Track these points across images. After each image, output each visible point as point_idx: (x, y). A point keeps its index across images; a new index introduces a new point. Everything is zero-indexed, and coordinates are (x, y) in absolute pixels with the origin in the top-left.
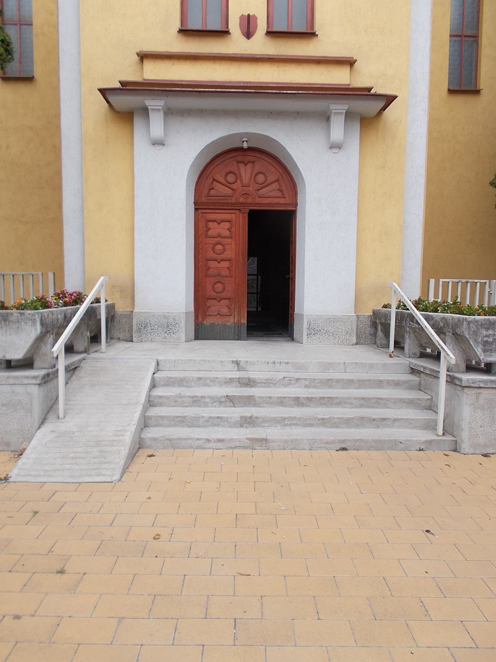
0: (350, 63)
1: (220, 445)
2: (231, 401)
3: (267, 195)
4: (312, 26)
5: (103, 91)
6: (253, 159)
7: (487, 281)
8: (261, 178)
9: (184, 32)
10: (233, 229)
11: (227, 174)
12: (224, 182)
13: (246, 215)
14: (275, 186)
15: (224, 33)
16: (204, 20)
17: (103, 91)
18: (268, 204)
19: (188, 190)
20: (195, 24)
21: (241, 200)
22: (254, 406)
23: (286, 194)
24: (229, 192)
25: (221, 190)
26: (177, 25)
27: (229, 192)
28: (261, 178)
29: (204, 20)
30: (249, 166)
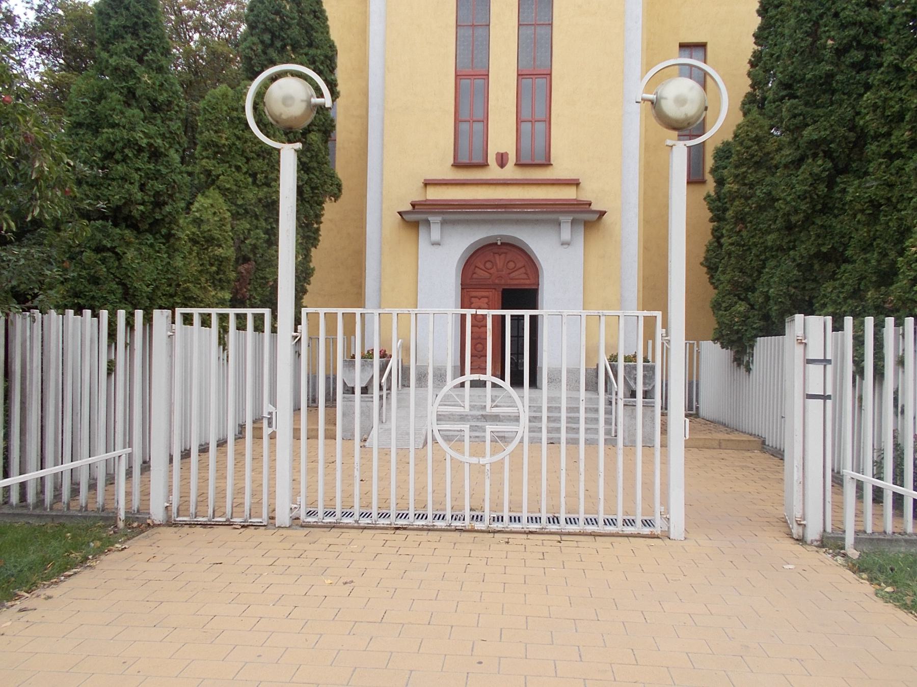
0: (576, 183)
1: (477, 439)
2: (484, 418)
3: (517, 277)
4: (549, 160)
5: (400, 213)
6: (505, 251)
7: (695, 342)
8: (511, 265)
9: (457, 165)
10: (490, 303)
11: (485, 263)
12: (483, 268)
13: (500, 293)
14: (523, 270)
15: (484, 165)
16: (471, 158)
17: (400, 213)
18: (517, 285)
19: (456, 276)
20: (465, 160)
21: (497, 281)
22: (499, 421)
23: (531, 277)
24: (486, 275)
25: (481, 274)
26: (452, 162)
27: (486, 275)
28: (511, 265)
29: (471, 158)
30: (503, 256)
